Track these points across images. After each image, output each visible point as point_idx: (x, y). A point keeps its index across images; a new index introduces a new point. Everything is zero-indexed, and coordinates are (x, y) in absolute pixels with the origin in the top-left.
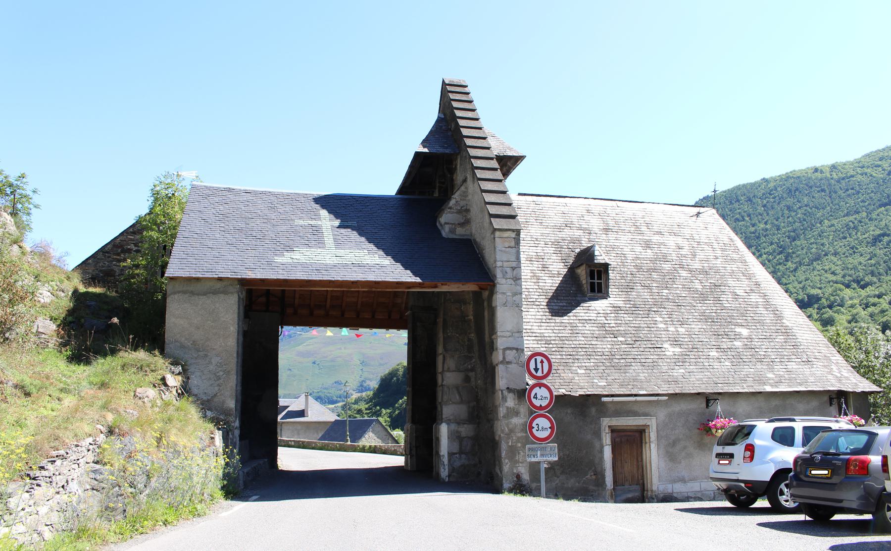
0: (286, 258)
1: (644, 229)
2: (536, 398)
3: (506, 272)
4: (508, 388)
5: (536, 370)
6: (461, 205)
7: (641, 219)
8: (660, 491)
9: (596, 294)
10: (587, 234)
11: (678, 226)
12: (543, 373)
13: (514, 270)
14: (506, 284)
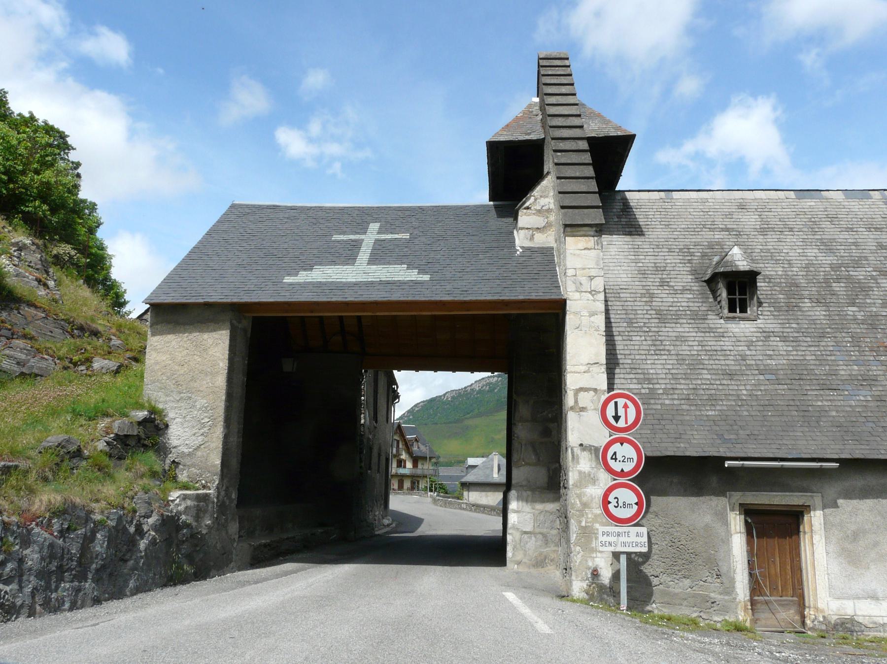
2: (616, 459)
3: (581, 284)
4: (581, 445)
5: (617, 418)
8: (832, 611)
9: (738, 314)
11: (883, 218)
12: (626, 423)
13: (591, 280)
14: (580, 300)
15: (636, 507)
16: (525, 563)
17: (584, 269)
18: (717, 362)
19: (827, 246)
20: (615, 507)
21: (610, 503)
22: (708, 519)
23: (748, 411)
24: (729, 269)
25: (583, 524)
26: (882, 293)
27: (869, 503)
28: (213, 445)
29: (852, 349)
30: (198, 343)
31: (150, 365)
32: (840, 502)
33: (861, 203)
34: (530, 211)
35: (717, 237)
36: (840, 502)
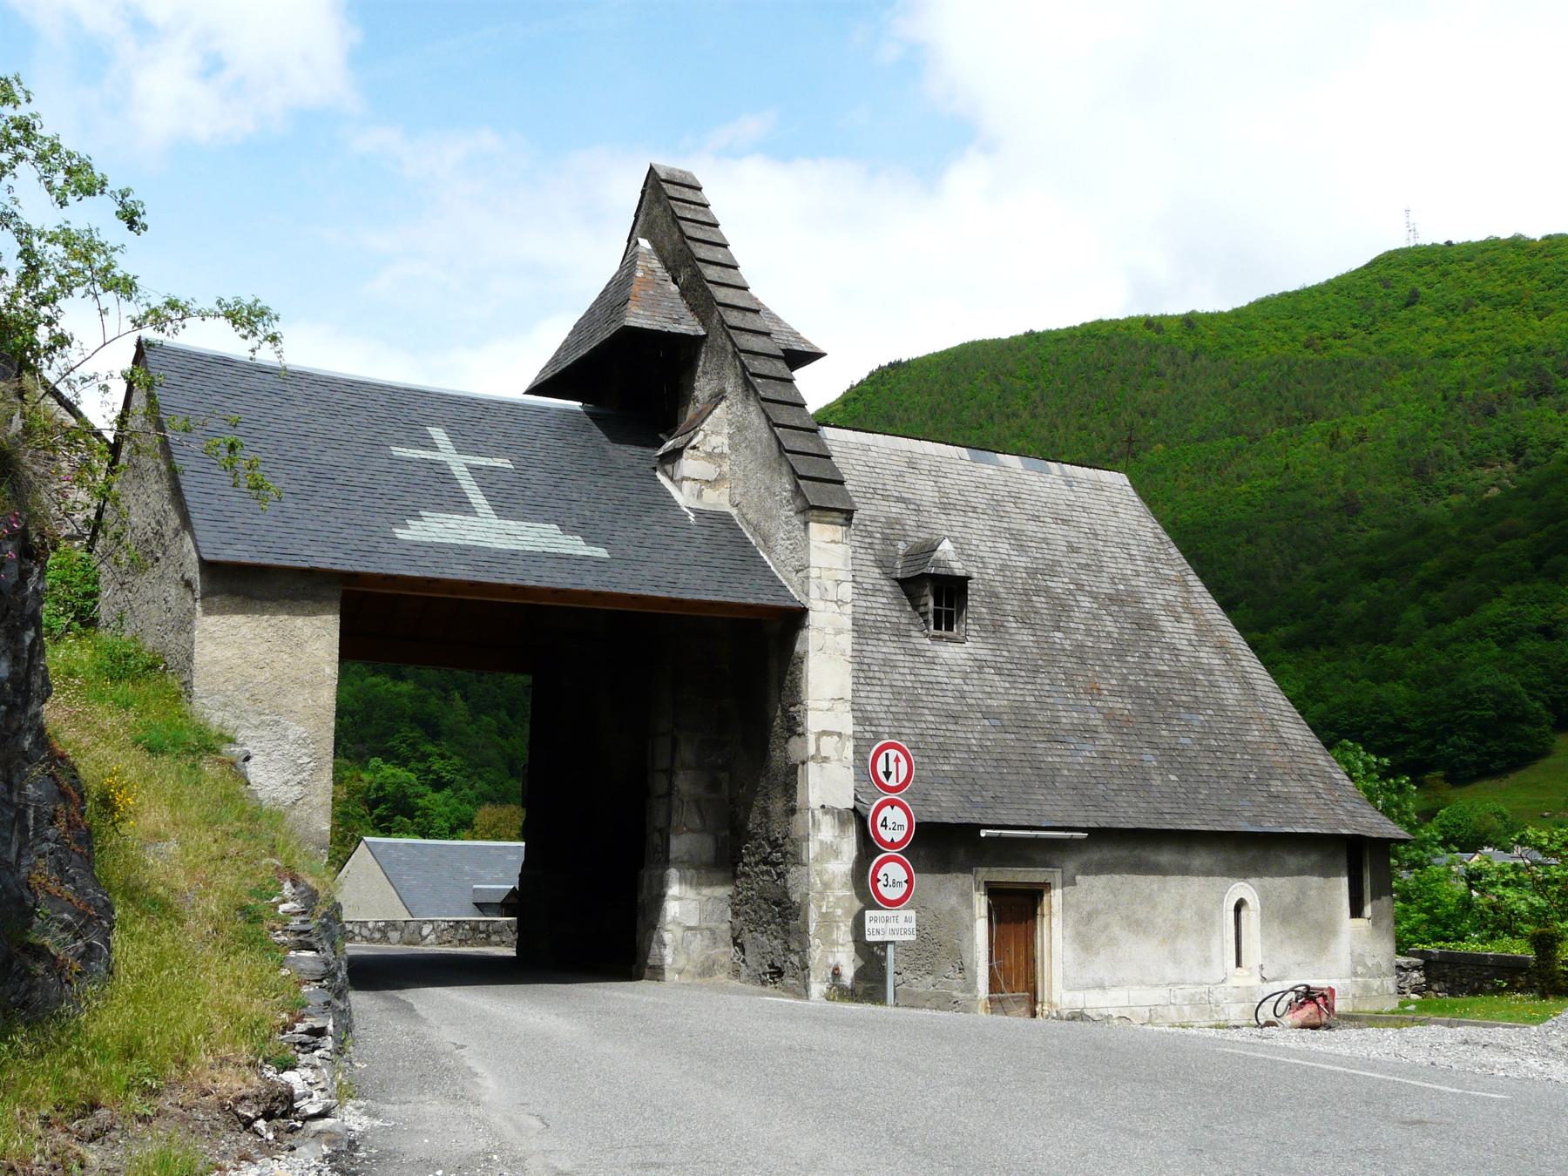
0: (412, 532)
1: (1010, 507)
2: (886, 826)
4: (823, 807)
5: (887, 774)
6: (714, 444)
7: (1002, 488)
9: (943, 632)
10: (913, 512)
15: (905, 885)
16: (688, 971)
17: (830, 569)
18: (936, 699)
19: (1018, 540)
20: (885, 886)
21: (879, 880)
22: (954, 900)
23: (983, 766)
24: (942, 571)
25: (824, 910)
26: (1083, 616)
27: (1103, 879)
28: (317, 801)
29: (1067, 689)
30: (286, 633)
31: (203, 665)
32: (1078, 878)
33: (1042, 479)
34: (698, 453)
35: (894, 510)
36: (1078, 878)
